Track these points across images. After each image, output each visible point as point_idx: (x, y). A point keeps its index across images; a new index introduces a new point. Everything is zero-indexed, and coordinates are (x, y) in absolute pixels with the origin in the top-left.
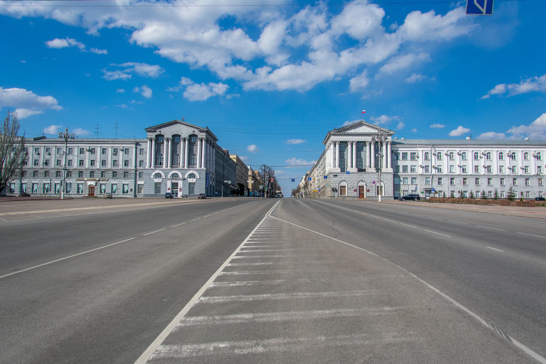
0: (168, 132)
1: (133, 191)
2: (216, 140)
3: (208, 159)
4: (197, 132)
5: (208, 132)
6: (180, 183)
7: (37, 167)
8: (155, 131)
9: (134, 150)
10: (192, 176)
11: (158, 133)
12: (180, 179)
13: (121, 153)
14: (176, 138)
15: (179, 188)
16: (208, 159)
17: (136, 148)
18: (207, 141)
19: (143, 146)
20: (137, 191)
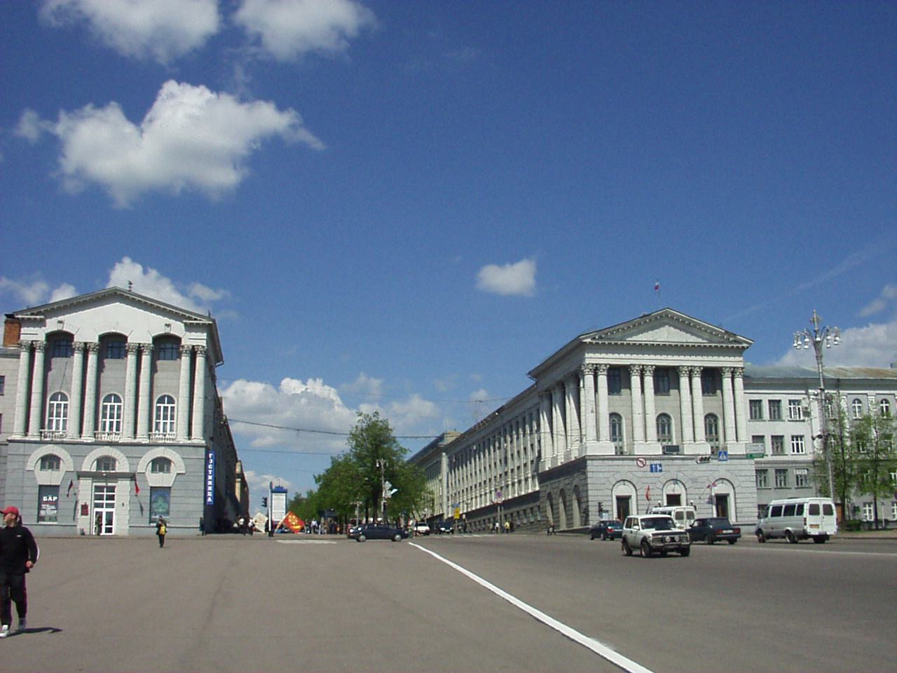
4: (177, 328)
5: (211, 330)
8: (41, 323)
10: (161, 464)
11: (52, 325)
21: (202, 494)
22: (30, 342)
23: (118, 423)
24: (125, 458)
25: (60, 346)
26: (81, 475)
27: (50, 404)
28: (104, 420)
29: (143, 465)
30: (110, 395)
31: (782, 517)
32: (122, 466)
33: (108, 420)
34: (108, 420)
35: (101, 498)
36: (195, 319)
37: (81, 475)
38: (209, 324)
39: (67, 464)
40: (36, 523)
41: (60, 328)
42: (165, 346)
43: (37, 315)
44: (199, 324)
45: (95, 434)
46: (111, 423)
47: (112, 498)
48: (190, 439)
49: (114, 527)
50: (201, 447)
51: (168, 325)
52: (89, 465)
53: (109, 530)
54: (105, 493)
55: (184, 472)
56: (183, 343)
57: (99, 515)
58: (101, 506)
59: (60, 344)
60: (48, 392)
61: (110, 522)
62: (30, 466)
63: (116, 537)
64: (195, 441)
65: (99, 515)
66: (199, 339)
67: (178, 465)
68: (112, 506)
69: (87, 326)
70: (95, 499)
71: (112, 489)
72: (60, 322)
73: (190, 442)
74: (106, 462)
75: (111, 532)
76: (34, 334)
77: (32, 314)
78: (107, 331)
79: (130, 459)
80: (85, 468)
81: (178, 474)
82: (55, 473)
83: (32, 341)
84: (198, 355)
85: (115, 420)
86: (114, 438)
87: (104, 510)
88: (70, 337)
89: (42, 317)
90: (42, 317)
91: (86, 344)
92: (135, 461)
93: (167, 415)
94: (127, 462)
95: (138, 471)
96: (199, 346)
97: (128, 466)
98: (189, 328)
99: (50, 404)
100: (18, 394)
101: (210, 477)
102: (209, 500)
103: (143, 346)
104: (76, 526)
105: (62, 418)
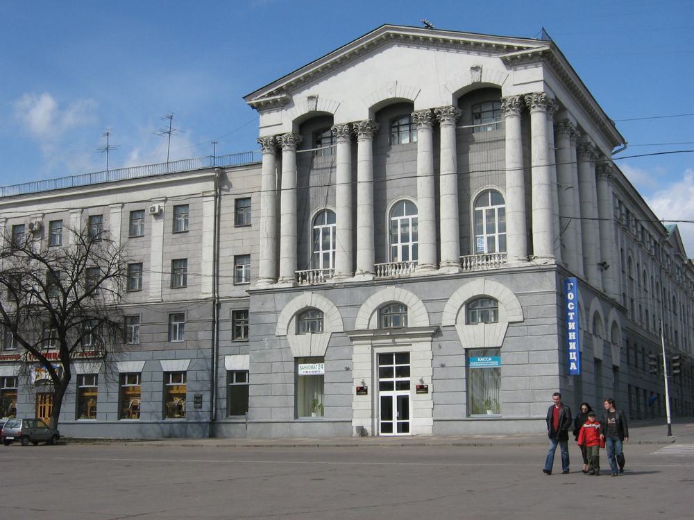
0: (348, 96)
1: (206, 405)
2: (614, 139)
3: (572, 209)
4: (493, 70)
5: (551, 60)
6: (421, 356)
7: (179, 295)
8: (286, 103)
9: (208, 206)
10: (480, 308)
11: (301, 106)
12: (418, 333)
13: (157, 229)
14: (391, 116)
15: (414, 380)
16: (572, 209)
17: (217, 197)
18: (555, 111)
19: (240, 182)
20: (471, 319)
21: (555, 356)
22: (272, 138)
23: (415, 248)
24: (421, 303)
25: (398, 127)
26: (354, 336)
27: (475, 212)
28: (393, 245)
29: (452, 312)
30: (485, 193)
31: (381, 421)
32: (418, 316)
33: (399, 245)
34: (399, 245)
35: (388, 372)
36: (528, 48)
37: (354, 336)
38: (544, 52)
39: (333, 321)
40: (116, 421)
41: (313, 109)
42: (477, 101)
43: (277, 94)
44: (527, 55)
45: (461, 261)
46: (405, 249)
47: (405, 372)
48: (529, 260)
49: (411, 421)
50: (550, 270)
51: (476, 69)
52: (365, 318)
53: (404, 428)
54: (394, 366)
55: (521, 318)
56: (504, 94)
57: (387, 402)
58: (388, 386)
59: (315, 128)
60: (388, 201)
61: (404, 413)
62: (281, 329)
63: (420, 442)
64: (538, 262)
65: (387, 402)
66: (526, 81)
67: (510, 308)
68: (405, 386)
69: (348, 96)
70: (381, 377)
71: (404, 357)
72: (311, 98)
73: (529, 264)
74: (391, 314)
75: (408, 431)
76: (281, 122)
77: (271, 94)
78: (390, 96)
79: (429, 304)
80: (361, 324)
81: (509, 323)
82: (317, 337)
83: (275, 137)
84: (532, 110)
85: (410, 244)
86: (403, 273)
87: (395, 394)
88: (327, 118)
89: (284, 96)
90: (284, 96)
91: (350, 125)
92: (436, 306)
93: (494, 225)
94: (424, 309)
95: (443, 325)
96: (531, 94)
97: (426, 316)
98: (511, 63)
99: (475, 212)
100: (262, 220)
101: (572, 326)
102: (573, 366)
103: (439, 113)
104: (351, 422)
105: (496, 235)
